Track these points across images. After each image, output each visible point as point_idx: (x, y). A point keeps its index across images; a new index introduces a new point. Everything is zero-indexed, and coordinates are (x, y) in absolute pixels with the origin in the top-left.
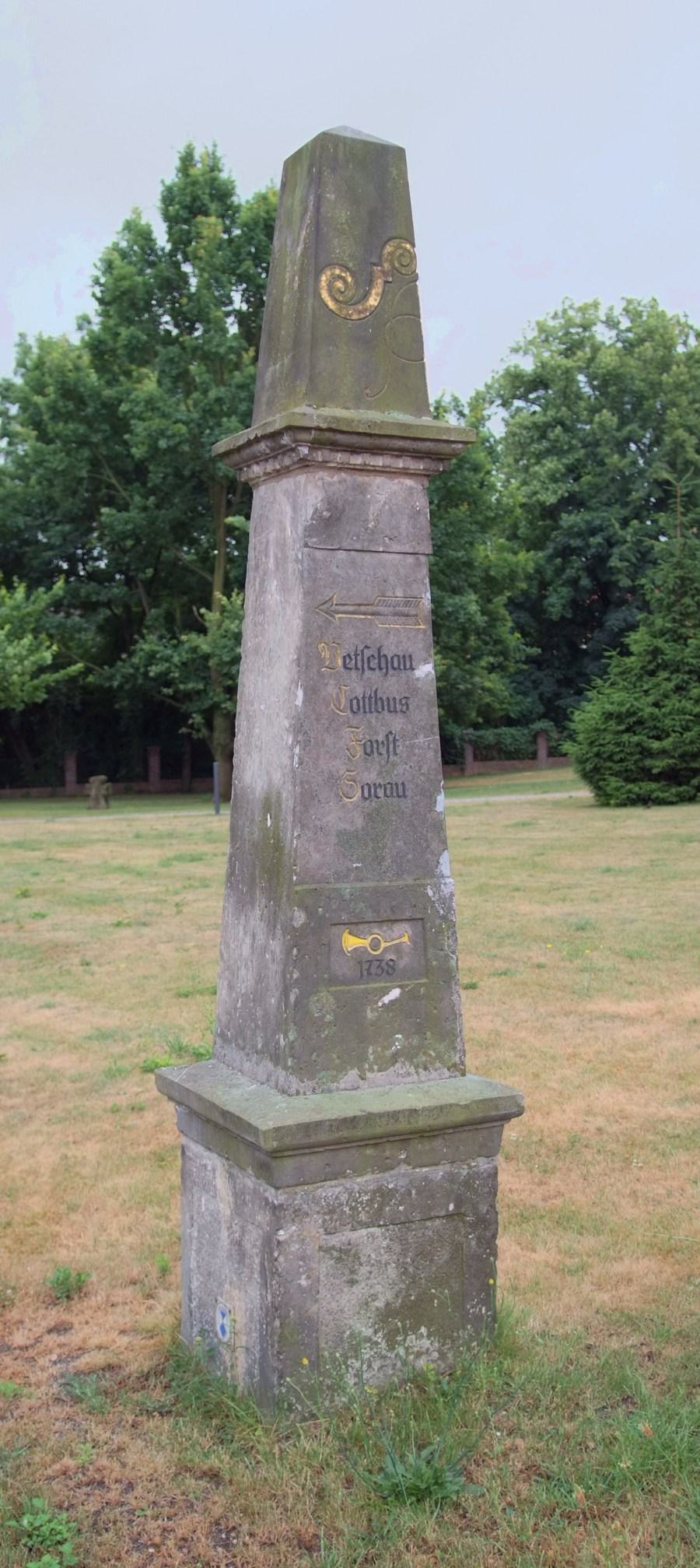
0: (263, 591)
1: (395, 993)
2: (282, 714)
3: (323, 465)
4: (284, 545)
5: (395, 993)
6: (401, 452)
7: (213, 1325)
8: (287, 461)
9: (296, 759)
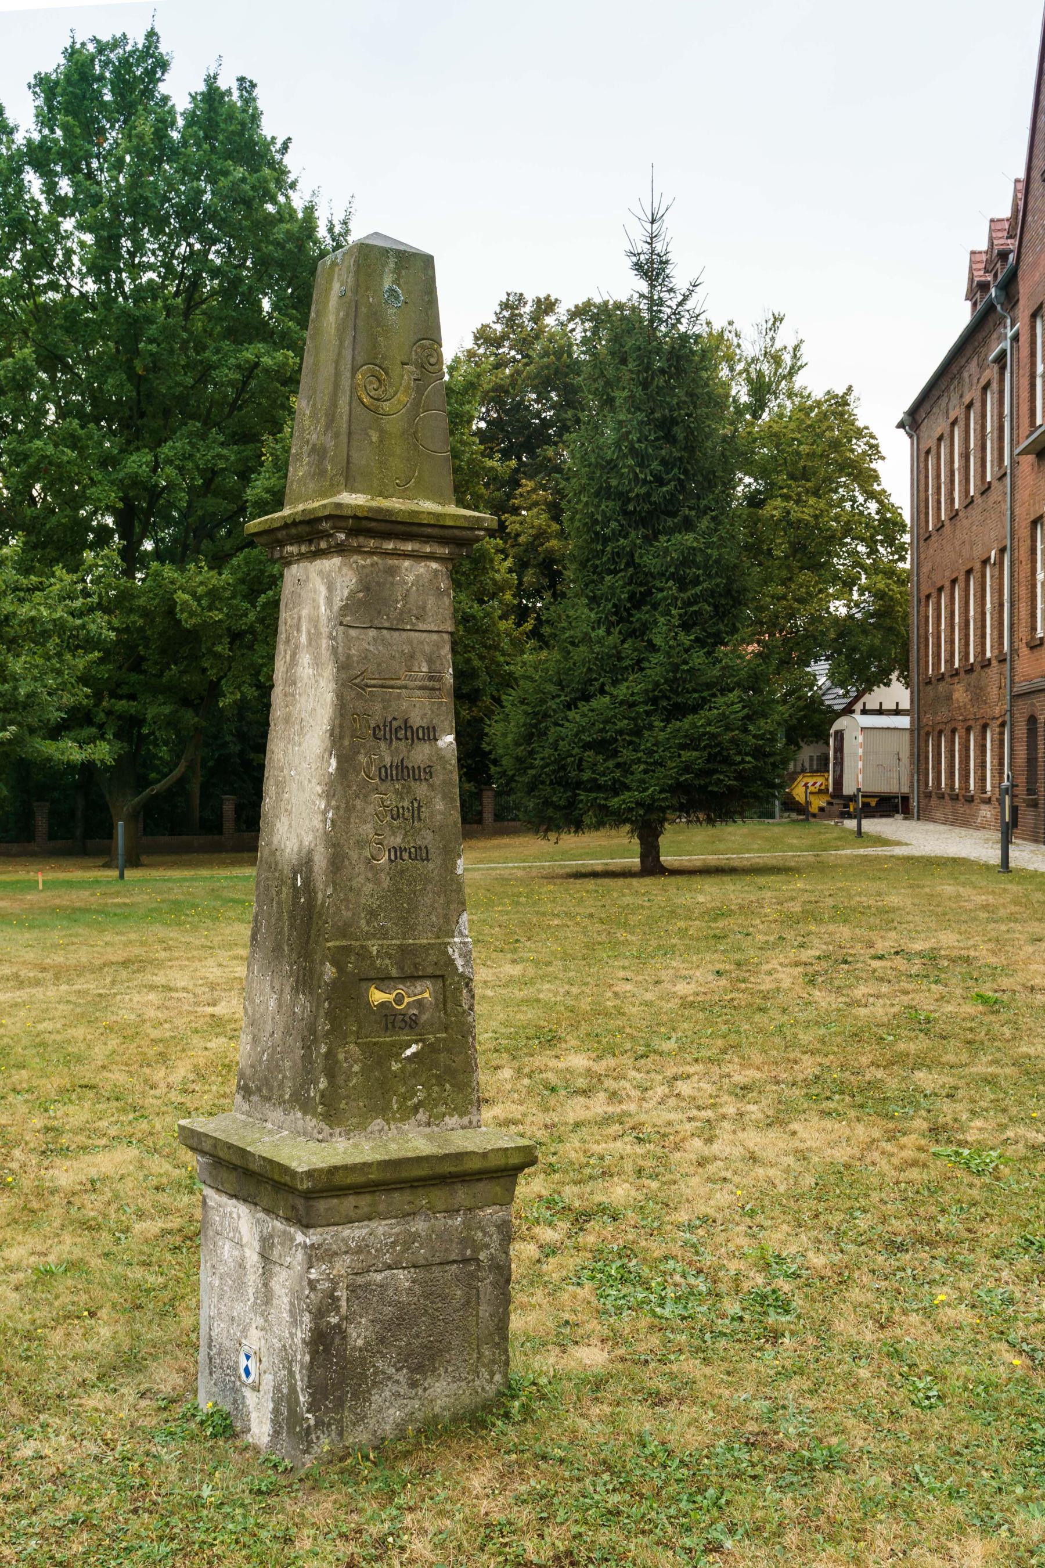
0: (294, 662)
1: (414, 1049)
2: (314, 781)
3: (358, 550)
4: (318, 621)
5: (414, 1049)
6: (428, 539)
7: (236, 1369)
8: (323, 545)
9: (329, 823)
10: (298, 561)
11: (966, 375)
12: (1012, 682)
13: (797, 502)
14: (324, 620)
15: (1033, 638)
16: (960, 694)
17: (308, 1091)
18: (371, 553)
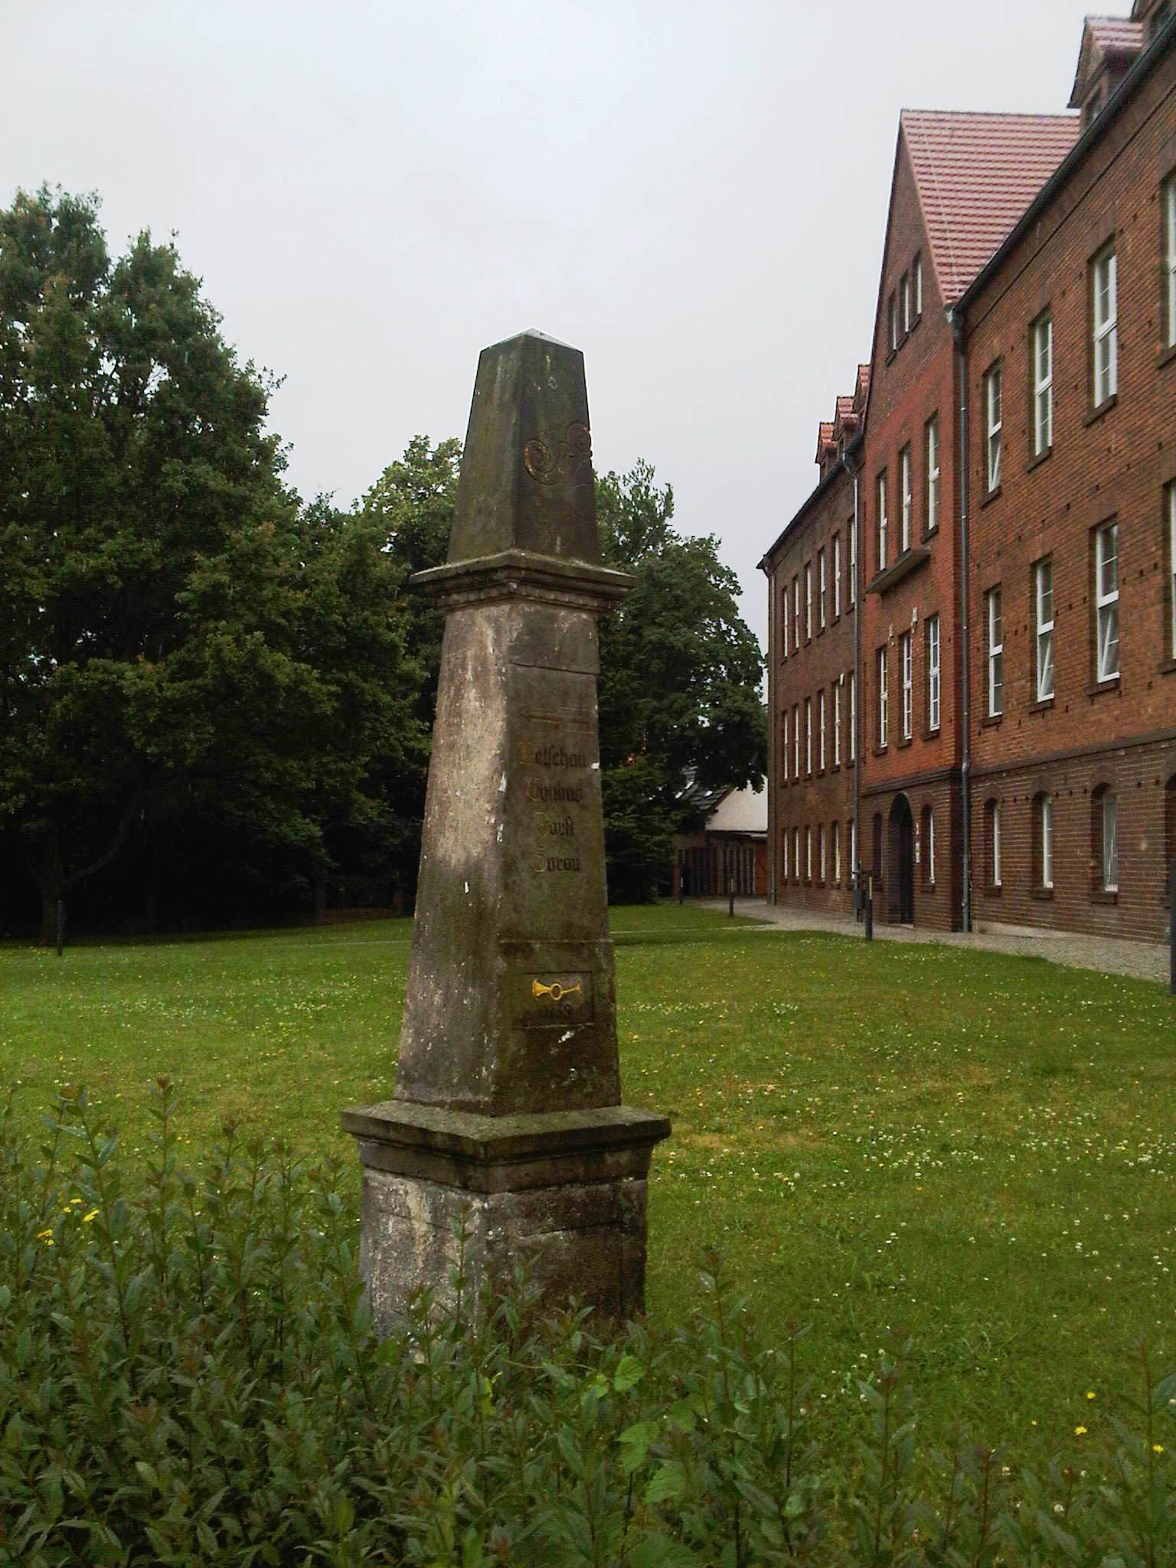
0: (459, 695)
1: (568, 1035)
3: (525, 599)
5: (568, 1035)
6: (582, 592)
8: (494, 593)
9: (500, 835)
10: (463, 608)
11: (818, 525)
12: (859, 786)
13: (671, 629)
14: (492, 658)
15: (878, 748)
16: (812, 795)
17: (479, 1073)
18: (536, 602)
